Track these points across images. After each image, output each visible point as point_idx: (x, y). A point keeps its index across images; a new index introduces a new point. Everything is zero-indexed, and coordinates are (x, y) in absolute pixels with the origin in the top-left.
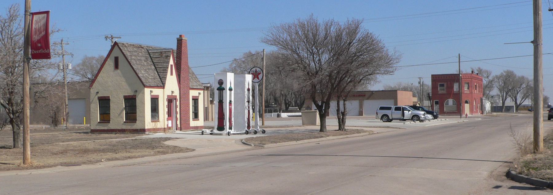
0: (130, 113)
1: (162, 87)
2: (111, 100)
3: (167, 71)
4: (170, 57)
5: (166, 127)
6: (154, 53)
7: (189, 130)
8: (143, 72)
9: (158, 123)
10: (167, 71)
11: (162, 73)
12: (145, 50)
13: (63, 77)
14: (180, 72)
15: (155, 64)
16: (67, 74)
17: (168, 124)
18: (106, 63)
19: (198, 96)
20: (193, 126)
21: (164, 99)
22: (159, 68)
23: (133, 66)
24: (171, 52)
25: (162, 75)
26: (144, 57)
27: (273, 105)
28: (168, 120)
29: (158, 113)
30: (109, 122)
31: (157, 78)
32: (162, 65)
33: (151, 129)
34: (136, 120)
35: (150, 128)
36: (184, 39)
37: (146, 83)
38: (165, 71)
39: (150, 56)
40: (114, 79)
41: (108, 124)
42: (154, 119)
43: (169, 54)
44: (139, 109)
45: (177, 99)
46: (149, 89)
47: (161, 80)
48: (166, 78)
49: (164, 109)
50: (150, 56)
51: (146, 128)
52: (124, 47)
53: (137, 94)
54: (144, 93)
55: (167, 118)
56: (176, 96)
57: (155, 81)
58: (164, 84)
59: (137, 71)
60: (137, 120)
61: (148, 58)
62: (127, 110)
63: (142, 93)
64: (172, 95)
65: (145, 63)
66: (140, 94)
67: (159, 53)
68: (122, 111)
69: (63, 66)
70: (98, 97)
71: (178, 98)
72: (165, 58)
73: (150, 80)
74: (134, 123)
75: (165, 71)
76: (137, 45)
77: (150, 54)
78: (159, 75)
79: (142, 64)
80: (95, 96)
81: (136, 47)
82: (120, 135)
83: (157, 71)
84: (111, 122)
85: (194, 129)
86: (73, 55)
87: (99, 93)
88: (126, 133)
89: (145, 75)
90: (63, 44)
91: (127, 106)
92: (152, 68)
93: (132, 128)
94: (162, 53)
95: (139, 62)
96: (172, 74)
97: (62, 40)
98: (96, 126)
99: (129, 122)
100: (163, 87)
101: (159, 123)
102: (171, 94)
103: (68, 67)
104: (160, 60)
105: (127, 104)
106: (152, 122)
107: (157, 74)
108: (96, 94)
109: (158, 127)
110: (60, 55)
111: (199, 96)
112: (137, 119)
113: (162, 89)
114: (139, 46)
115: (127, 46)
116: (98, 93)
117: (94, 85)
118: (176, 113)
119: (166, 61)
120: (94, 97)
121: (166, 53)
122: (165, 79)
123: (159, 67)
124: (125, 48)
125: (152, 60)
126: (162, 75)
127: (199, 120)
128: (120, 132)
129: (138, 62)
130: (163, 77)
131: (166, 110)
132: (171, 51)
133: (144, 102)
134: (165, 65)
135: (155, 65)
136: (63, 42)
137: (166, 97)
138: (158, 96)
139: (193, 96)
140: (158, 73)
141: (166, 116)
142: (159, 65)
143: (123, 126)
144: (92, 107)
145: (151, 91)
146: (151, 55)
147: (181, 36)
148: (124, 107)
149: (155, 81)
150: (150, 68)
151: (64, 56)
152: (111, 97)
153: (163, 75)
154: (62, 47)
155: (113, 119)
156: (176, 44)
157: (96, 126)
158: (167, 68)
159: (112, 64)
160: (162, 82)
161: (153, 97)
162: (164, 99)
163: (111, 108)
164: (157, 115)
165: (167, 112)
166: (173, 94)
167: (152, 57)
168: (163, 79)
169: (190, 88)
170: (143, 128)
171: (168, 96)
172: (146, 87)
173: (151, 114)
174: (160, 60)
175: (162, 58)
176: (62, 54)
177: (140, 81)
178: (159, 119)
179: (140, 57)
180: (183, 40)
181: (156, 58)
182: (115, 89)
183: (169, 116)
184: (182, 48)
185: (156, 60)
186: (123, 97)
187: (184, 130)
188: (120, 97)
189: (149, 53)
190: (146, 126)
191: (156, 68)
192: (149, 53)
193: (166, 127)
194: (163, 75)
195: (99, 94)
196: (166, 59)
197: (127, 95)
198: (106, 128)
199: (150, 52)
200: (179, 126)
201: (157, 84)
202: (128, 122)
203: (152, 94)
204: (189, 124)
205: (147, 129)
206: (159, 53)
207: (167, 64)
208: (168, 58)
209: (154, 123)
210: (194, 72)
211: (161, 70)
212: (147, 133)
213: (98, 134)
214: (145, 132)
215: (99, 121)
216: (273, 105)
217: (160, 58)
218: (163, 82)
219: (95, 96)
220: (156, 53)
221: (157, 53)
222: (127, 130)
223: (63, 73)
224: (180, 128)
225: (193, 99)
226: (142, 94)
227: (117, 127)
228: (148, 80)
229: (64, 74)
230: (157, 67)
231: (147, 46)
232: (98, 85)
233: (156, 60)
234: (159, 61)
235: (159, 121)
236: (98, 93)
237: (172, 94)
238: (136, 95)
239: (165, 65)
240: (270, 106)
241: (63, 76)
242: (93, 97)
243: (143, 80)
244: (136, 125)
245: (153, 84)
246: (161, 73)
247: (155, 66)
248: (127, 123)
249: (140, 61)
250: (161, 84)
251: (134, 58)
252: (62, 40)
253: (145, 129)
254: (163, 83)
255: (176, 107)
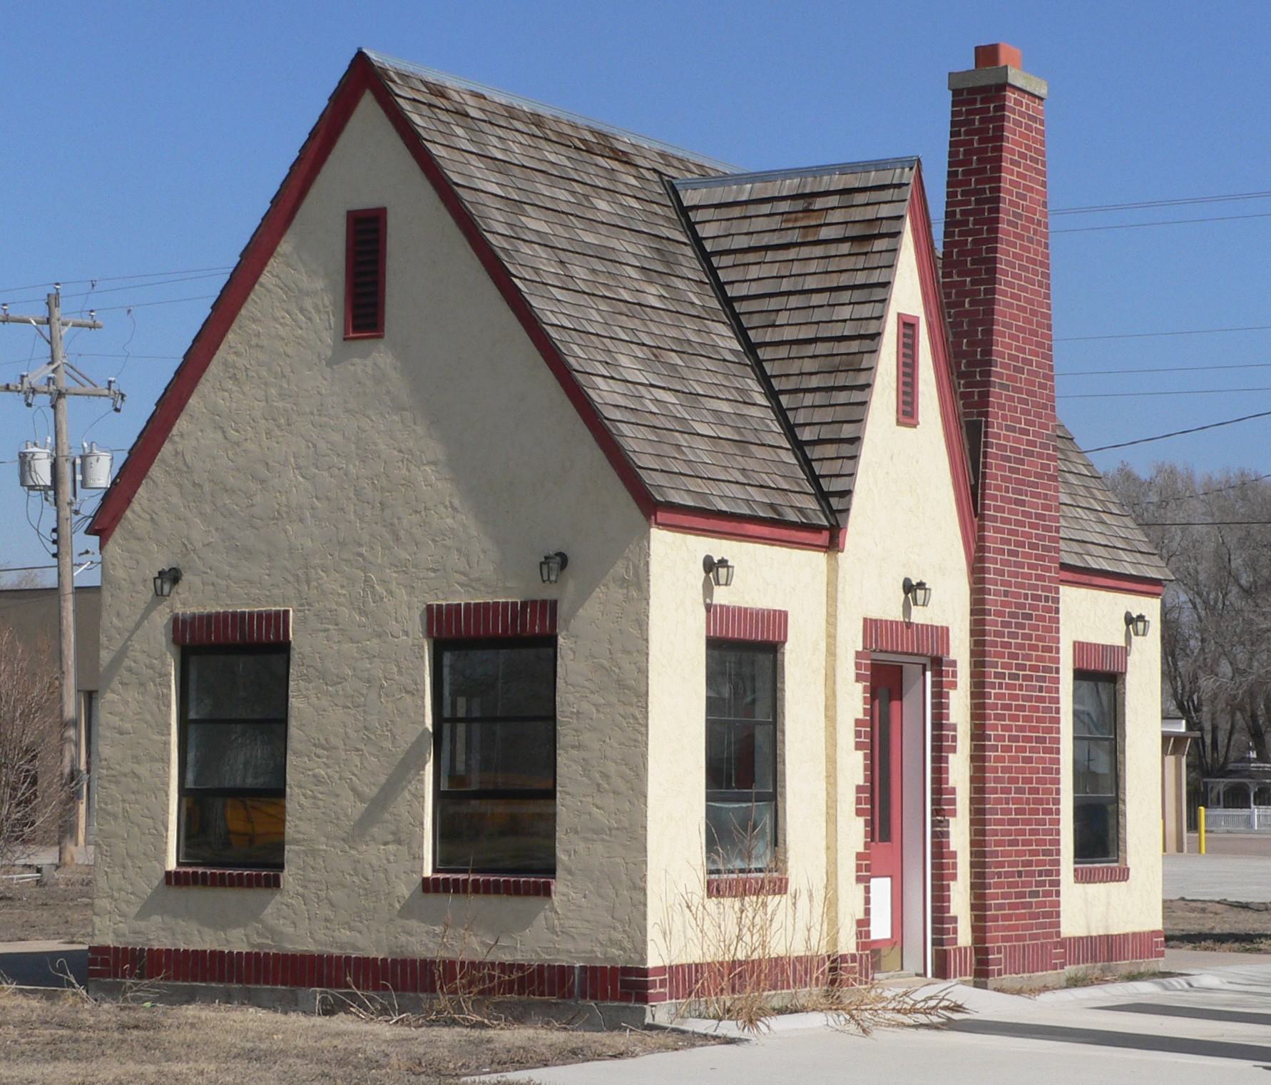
0: (481, 795)
1: (817, 529)
2: (295, 656)
3: (862, 379)
4: (897, 234)
5: (848, 944)
6: (736, 212)
7: (1050, 976)
8: (628, 365)
9: (773, 901)
10: (862, 379)
11: (819, 398)
12: (640, 178)
13: (55, 536)
14: (985, 396)
15: (739, 307)
16: (77, 518)
17: (867, 912)
18: (265, 278)
19: (1120, 641)
20: (1080, 932)
21: (831, 653)
22: (783, 352)
23: (535, 302)
24: (908, 193)
25: (818, 416)
26: (643, 240)
27: (1250, 761)
28: (866, 871)
29: (773, 797)
30: (274, 883)
31: (769, 439)
32: (818, 315)
33: (698, 967)
34: (551, 871)
35: (693, 955)
36: (1019, 83)
37: (659, 479)
38: (842, 380)
39: (697, 242)
40: (337, 438)
41: (251, 896)
42: (738, 864)
43: (885, 211)
44: (579, 747)
45: (953, 664)
46: (692, 540)
47: (806, 463)
48: (856, 440)
49: (831, 762)
50: (697, 242)
51: (653, 961)
52: (444, 117)
53: (566, 592)
54: (638, 582)
55: (859, 856)
56: (941, 634)
57: (751, 464)
58: (834, 502)
59: (577, 355)
60: (560, 872)
61: (672, 247)
62: (461, 758)
63: (623, 583)
64: (909, 625)
65: (652, 295)
66: (598, 593)
67: (784, 206)
68: (410, 765)
69: (55, 467)
70: (175, 620)
71: (960, 650)
72: (845, 248)
73: (701, 452)
74: (533, 901)
75: (842, 380)
76: (574, 126)
77: (695, 216)
78: (781, 414)
79: (626, 296)
80: (145, 616)
81: (562, 141)
82: (367, 1027)
83: (765, 380)
84: (288, 876)
85: (1095, 969)
86: (123, 396)
87: (186, 577)
88: (443, 1001)
89: (656, 401)
90: (57, 325)
91: (461, 713)
92: (714, 346)
93: (507, 958)
94: (819, 203)
95: (593, 271)
96: (907, 413)
97: (52, 301)
98: (143, 914)
99: (477, 888)
100: (824, 538)
101: (786, 900)
102: (895, 614)
103: (83, 472)
104: (797, 268)
105: (461, 701)
106: (714, 890)
107: (761, 400)
108: (159, 594)
109: (777, 948)
110: (34, 391)
111: (1125, 651)
112: (561, 855)
113: (819, 558)
114: (589, 137)
115: (474, 113)
116: (172, 576)
117: (135, 505)
118: (936, 802)
119: (860, 278)
120: (138, 625)
121: (860, 198)
122: (846, 450)
123: (789, 334)
124: (459, 131)
125: (712, 271)
126: (818, 416)
127: (1123, 875)
128: (376, 988)
129: (580, 272)
130: (826, 433)
131: (853, 767)
132: (909, 177)
133: (644, 672)
134: (845, 312)
135: (745, 321)
136: (57, 313)
137: (851, 640)
138: (779, 619)
139: (1080, 647)
140: (772, 394)
141: (853, 832)
142: (782, 318)
143: (413, 924)
144: (116, 721)
145: (711, 566)
146: (704, 231)
147: (987, 55)
148: (429, 722)
149: (751, 464)
150: (694, 338)
151: (63, 403)
152: (303, 621)
153: (828, 414)
154: (50, 343)
155: (314, 853)
156: (946, 138)
157: (143, 914)
158: (866, 345)
159: (319, 284)
160: (814, 479)
161: (734, 633)
162: (831, 653)
163: (293, 731)
164: (767, 819)
165: (859, 789)
166: (919, 616)
167: (709, 246)
168: (830, 450)
169: (1064, 567)
170: (619, 957)
171: (871, 626)
172: (661, 516)
173: (707, 807)
174: (797, 268)
175: (818, 251)
176: (52, 387)
177: (599, 454)
178: (779, 861)
179: (603, 229)
180: (1010, 94)
181: (751, 257)
182: (342, 544)
183: (871, 835)
184: (999, 169)
185: (754, 272)
186: (416, 626)
187: (1008, 979)
188: (394, 627)
189: (683, 211)
190: (653, 933)
191: (751, 348)
192: (683, 211)
193: (848, 944)
194: (828, 414)
195: (182, 587)
196: (860, 262)
197: (461, 599)
198: (237, 941)
199: (689, 198)
200: (964, 937)
201: (778, 499)
202: (459, 888)
203: (722, 596)
204: (1054, 915)
205: (661, 970)
206: (784, 206)
207: (866, 311)
208: (879, 245)
209: (730, 904)
210: (1074, 432)
211: (808, 366)
212: (660, 1013)
213: (161, 998)
214: (644, 999)
215: (172, 865)
216: (1255, 760)
217: (792, 253)
218: (827, 485)
219: (145, 616)
220: (752, 210)
221: (766, 209)
222: (449, 965)
223: (50, 512)
224: (971, 960)
225: (1080, 675)
226: (618, 594)
227: (345, 935)
228: (678, 447)
229: (58, 521)
230: (769, 336)
231: (662, 155)
232: (175, 500)
233: (754, 272)
234: (786, 285)
235: (780, 887)
236: (172, 576)
237: (907, 609)
238: (548, 609)
239: (845, 312)
240: (1231, 766)
241: (54, 530)
242: (130, 624)
243: (633, 439)
244: (540, 921)
245: (736, 491)
246: (809, 399)
247: (741, 333)
248: (449, 901)
249: (598, 265)
250: (811, 504)
251: (544, 228)
252: (52, 301)
253: (644, 972)
254: (823, 496)
255: (938, 739)
